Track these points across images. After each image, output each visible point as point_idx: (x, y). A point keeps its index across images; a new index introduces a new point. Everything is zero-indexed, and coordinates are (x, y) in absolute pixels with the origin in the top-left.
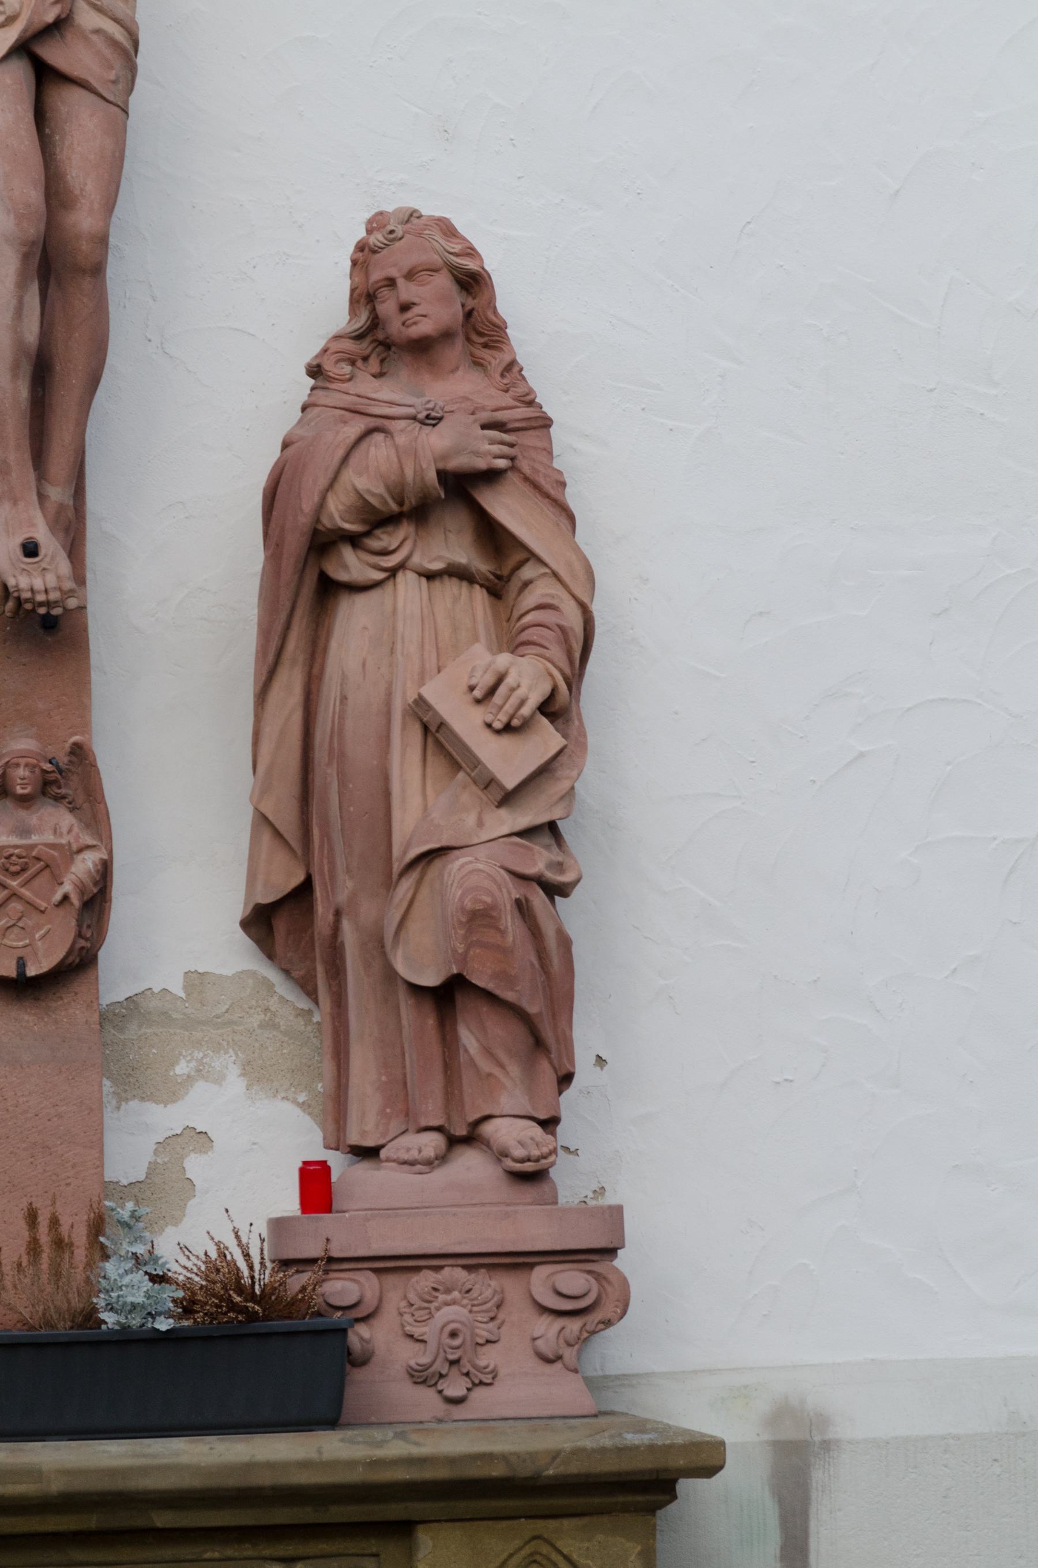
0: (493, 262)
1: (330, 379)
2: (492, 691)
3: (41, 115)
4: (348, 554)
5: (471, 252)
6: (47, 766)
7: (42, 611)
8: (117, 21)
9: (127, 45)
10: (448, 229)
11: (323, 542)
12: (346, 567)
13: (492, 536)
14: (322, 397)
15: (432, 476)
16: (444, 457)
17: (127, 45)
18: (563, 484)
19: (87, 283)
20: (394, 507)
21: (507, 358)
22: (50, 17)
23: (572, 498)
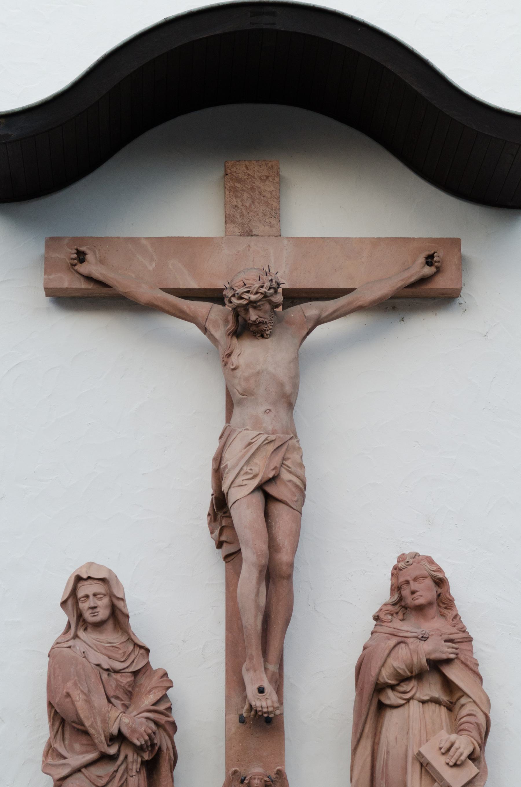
0: (449, 574)
1: (383, 621)
2: (449, 750)
3: (267, 514)
4: (390, 693)
5: (440, 570)
6: (267, 779)
7: (266, 715)
8: (298, 477)
9: (301, 486)
10: (430, 561)
11: (380, 688)
12: (389, 698)
13: (449, 686)
14: (379, 629)
15: (424, 661)
16: (430, 653)
17: (301, 486)
18: (477, 665)
19: (285, 582)
20: (409, 674)
21: (455, 613)
22: (271, 475)
23: (481, 670)
